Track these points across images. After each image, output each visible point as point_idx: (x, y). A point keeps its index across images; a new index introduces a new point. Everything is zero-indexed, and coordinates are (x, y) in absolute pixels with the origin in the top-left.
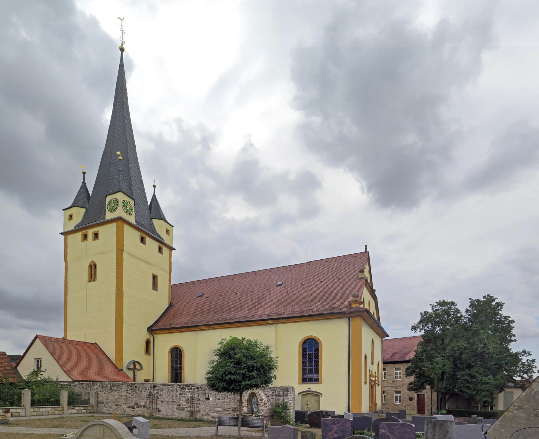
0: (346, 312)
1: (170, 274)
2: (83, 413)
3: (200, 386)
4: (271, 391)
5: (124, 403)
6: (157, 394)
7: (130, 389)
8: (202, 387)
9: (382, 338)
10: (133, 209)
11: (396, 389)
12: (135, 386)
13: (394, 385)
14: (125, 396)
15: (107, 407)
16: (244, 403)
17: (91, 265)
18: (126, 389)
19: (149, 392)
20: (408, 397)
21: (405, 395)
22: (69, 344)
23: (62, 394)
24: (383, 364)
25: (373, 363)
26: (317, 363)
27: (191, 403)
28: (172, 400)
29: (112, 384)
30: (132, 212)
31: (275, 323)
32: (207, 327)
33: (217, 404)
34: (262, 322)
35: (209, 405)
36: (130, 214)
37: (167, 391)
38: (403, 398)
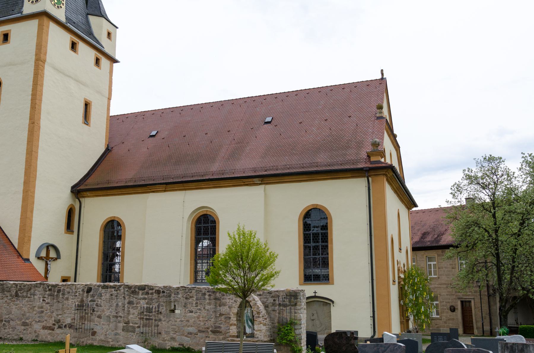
0: (364, 169)
4: (272, 297)
5: (37, 321)
6: (92, 303)
7: (49, 295)
8: (165, 291)
9: (409, 208)
12: (56, 289)
16: (232, 319)
18: (41, 294)
20: (448, 306)
21: (445, 302)
26: (325, 248)
27: (147, 319)
28: (117, 313)
30: (62, 5)
31: (263, 182)
32: (163, 187)
33: (188, 321)
34: (244, 180)
35: (176, 321)
36: (59, 8)
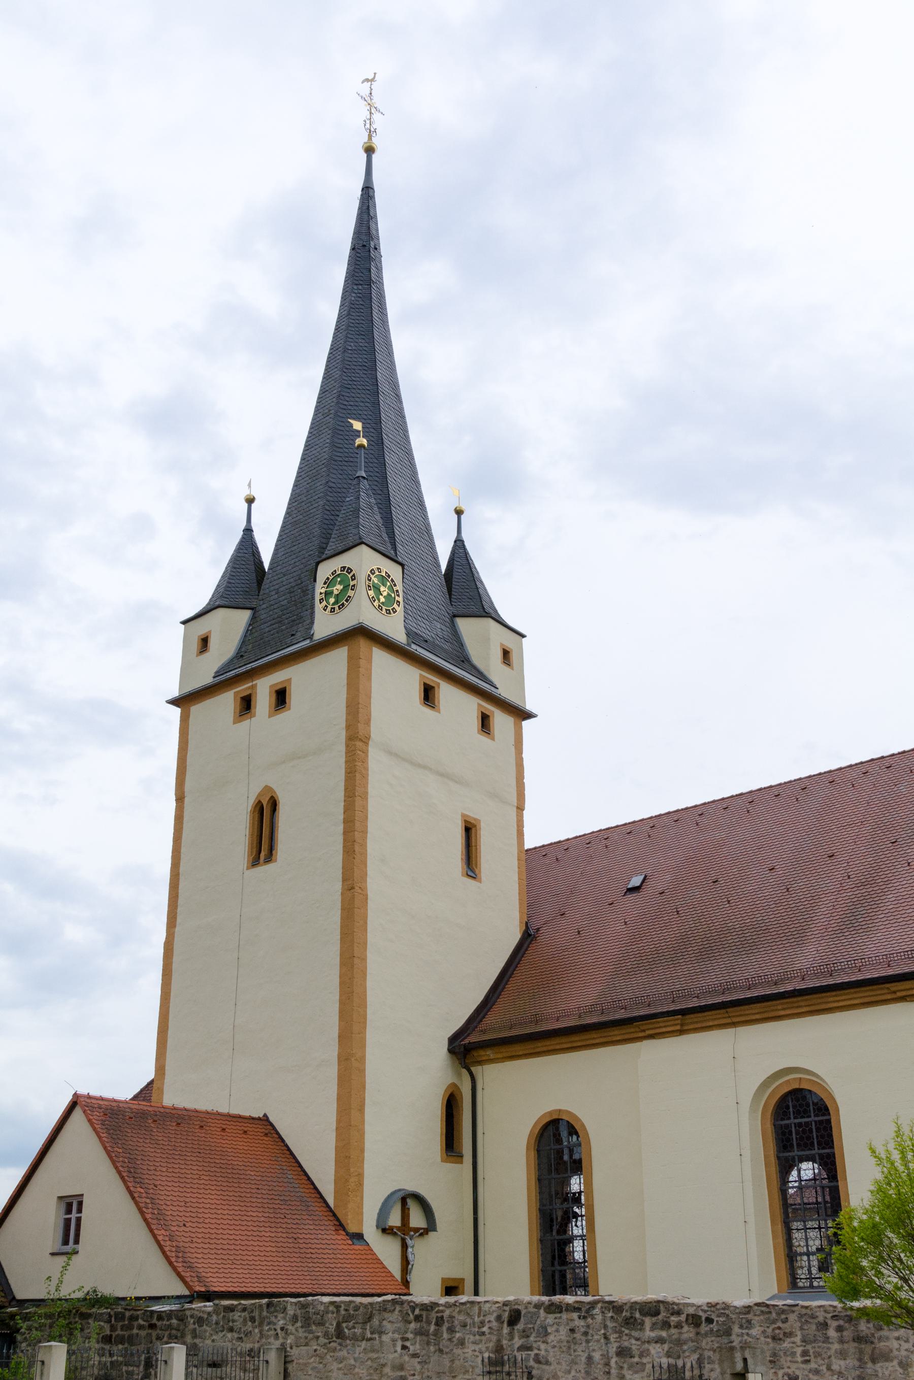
6: (524, 1353)
8: (714, 1317)
10: (398, 596)
12: (433, 1315)
17: (260, 802)
19: (491, 1345)
29: (343, 1307)
34: (894, 986)
36: (390, 613)
37: (563, 1338)
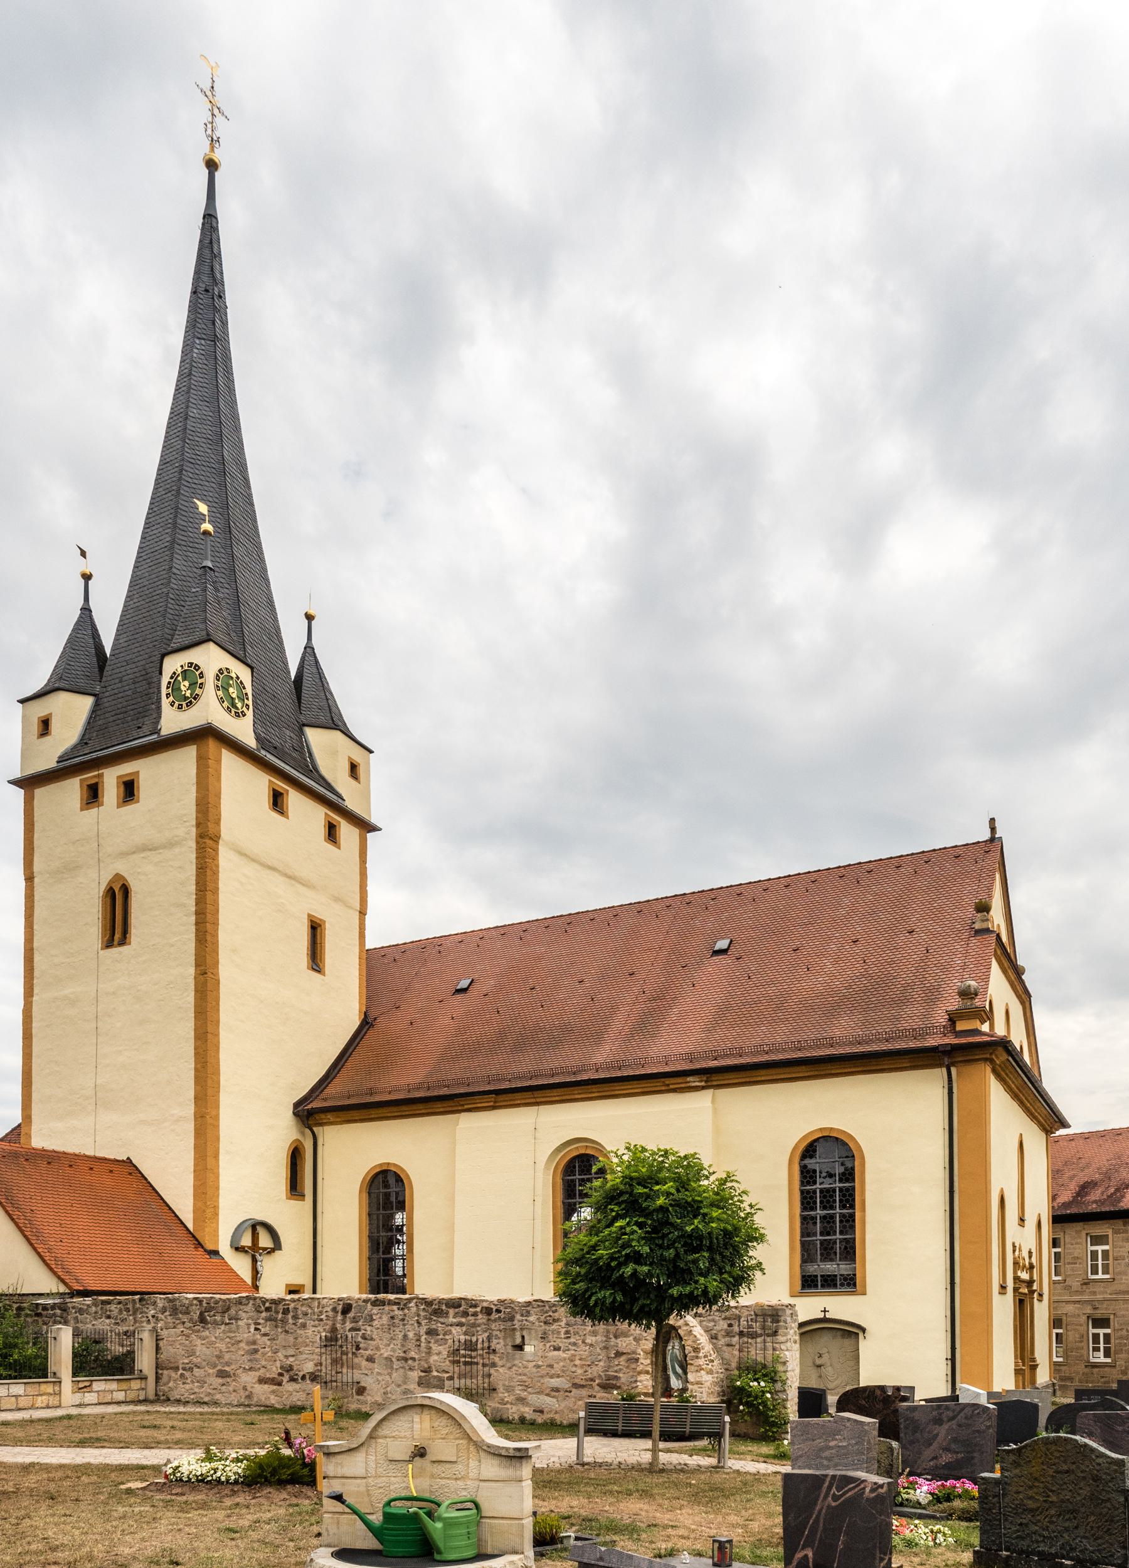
1: (363, 913)
2: (115, 1403)
3: (495, 1305)
5: (247, 1367)
6: (354, 1333)
7: (267, 1319)
9: (1048, 1131)
11: (1095, 1309)
12: (281, 1307)
13: (1086, 1297)
14: (249, 1343)
15: (189, 1381)
16: (641, 1361)
19: (327, 1327)
22: (49, 1163)
23: (55, 1338)
24: (1054, 1222)
25: (1022, 1220)
27: (466, 1363)
28: (405, 1352)
31: (709, 1084)
32: (490, 1100)
33: (551, 1366)
34: (668, 1081)
35: (526, 1367)
38: (1117, 1341)
